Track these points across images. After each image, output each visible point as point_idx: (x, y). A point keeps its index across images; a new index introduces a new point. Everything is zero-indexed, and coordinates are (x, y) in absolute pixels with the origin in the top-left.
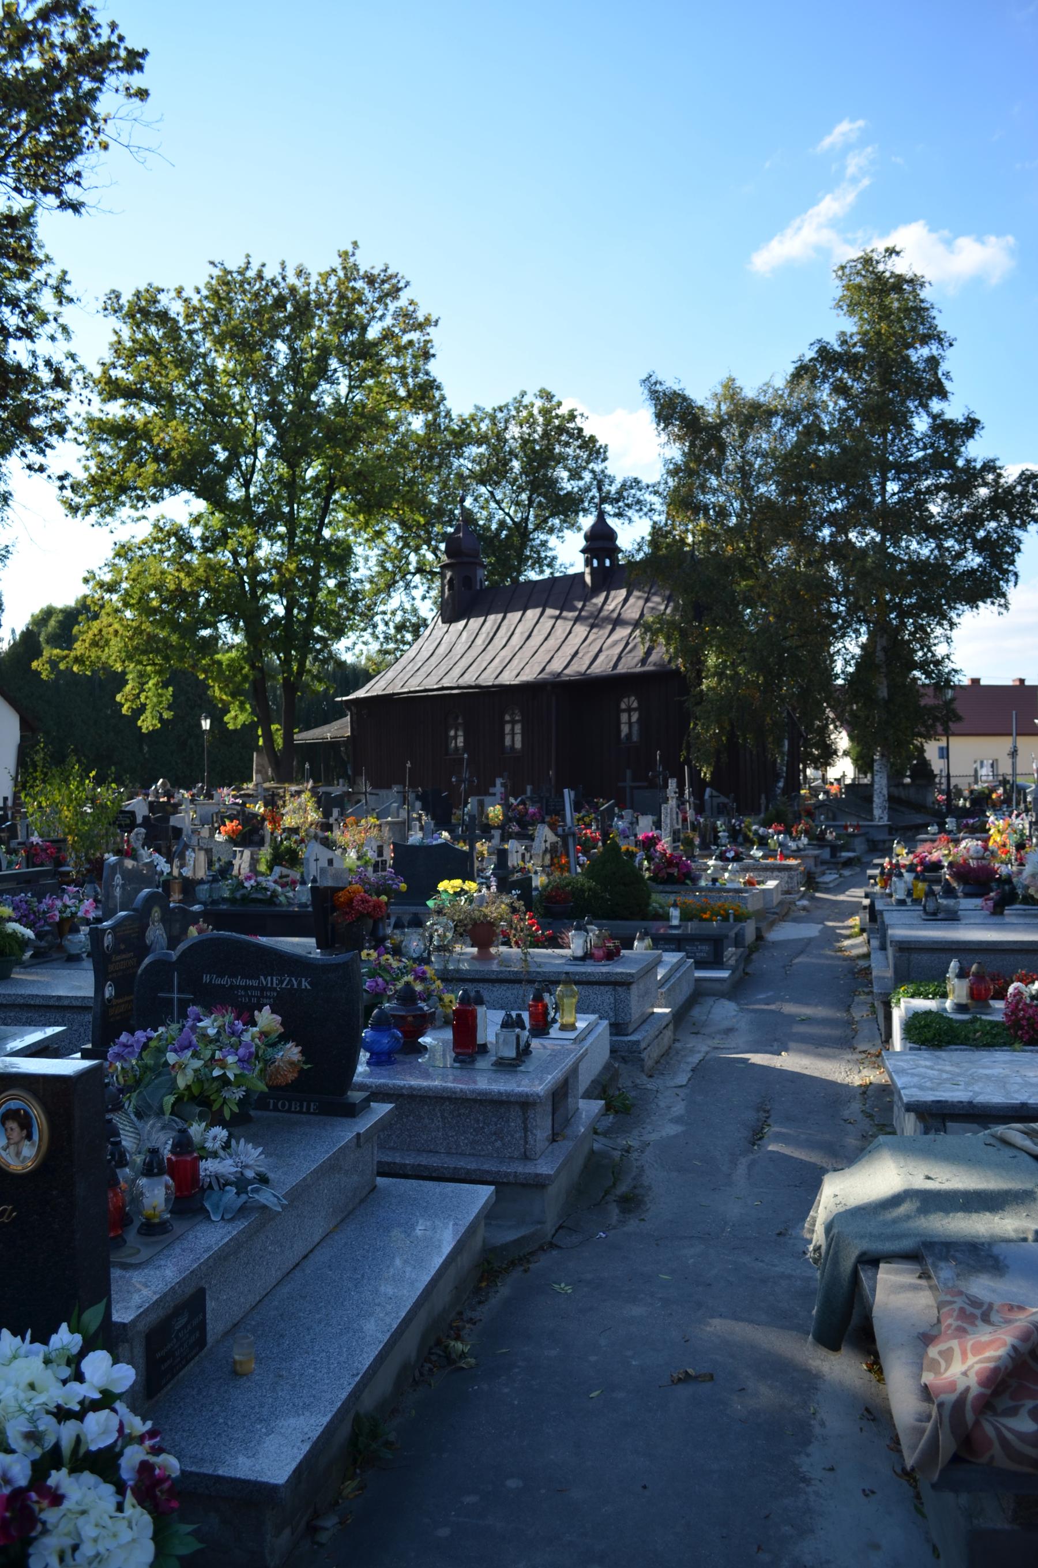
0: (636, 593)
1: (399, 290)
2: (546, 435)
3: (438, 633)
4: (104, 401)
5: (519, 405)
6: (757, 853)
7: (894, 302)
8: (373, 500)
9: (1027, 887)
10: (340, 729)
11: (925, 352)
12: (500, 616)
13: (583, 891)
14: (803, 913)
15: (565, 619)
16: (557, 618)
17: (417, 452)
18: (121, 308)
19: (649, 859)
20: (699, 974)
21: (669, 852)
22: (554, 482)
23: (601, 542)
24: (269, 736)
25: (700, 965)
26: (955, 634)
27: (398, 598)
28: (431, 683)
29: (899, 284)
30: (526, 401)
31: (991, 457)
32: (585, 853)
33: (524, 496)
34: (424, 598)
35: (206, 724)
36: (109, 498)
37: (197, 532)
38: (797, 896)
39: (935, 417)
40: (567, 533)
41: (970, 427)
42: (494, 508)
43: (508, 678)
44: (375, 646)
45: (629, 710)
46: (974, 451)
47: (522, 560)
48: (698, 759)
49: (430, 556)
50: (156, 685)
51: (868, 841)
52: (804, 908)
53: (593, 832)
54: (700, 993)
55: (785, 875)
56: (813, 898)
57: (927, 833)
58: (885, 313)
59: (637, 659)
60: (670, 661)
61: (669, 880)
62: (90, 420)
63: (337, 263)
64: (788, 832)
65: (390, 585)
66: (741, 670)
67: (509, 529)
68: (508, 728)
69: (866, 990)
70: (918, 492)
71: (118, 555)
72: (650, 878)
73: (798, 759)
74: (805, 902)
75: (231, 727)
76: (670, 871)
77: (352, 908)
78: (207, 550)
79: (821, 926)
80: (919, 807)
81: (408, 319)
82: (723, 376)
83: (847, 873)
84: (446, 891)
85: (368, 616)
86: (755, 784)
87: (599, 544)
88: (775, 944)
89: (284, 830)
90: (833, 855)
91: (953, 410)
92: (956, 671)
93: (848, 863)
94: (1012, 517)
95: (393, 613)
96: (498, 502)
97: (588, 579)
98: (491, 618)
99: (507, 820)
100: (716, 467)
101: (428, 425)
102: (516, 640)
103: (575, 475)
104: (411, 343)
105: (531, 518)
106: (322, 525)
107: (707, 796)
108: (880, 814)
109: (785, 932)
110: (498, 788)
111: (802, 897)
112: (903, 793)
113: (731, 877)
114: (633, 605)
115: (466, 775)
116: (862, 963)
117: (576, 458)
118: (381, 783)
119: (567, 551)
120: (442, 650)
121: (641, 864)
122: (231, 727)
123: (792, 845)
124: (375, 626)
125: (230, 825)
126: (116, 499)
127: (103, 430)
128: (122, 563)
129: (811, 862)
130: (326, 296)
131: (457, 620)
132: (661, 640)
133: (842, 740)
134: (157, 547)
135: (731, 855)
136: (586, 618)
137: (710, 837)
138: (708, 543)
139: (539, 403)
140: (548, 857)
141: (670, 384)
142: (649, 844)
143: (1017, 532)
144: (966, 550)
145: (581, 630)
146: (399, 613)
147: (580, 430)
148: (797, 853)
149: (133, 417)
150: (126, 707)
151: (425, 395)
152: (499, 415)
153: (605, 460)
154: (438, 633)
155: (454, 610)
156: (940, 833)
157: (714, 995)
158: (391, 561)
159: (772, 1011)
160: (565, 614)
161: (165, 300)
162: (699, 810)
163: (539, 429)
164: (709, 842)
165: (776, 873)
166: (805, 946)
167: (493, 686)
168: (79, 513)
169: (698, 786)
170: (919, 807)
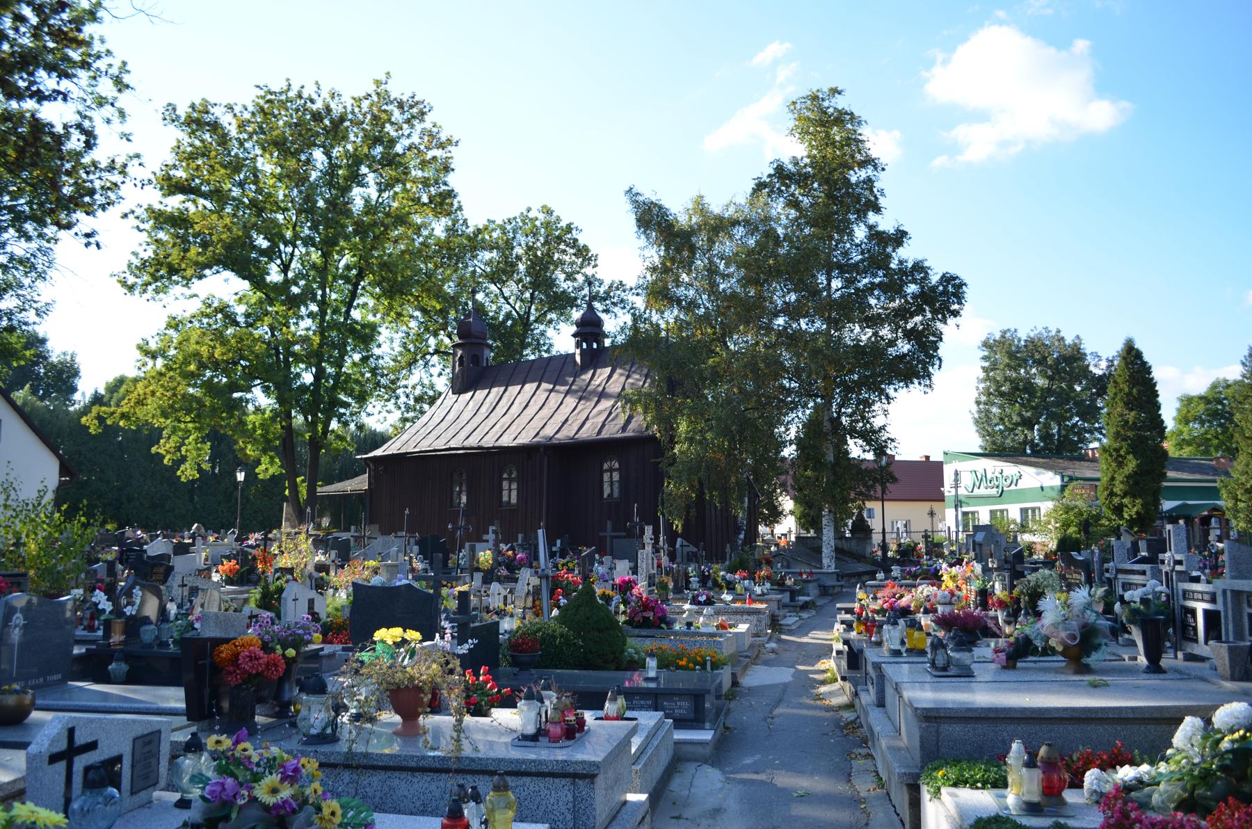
0: (619, 371)
1: (423, 114)
2: (546, 243)
3: (448, 403)
4: (164, 195)
5: (525, 219)
6: (727, 597)
7: (837, 134)
8: (395, 288)
9: (1047, 639)
10: (360, 483)
11: (863, 174)
12: (503, 389)
13: (554, 637)
14: (773, 656)
15: (558, 392)
16: (551, 391)
17: (439, 251)
18: (178, 117)
19: (625, 602)
20: (680, 735)
21: (644, 595)
22: (551, 283)
23: (589, 329)
24: (294, 488)
25: (680, 723)
26: (890, 408)
27: (418, 374)
28: (440, 444)
29: (841, 118)
30: (531, 215)
31: (920, 258)
32: (566, 596)
33: (527, 295)
34: (440, 374)
35: (241, 477)
36: (162, 277)
37: (240, 309)
38: (765, 639)
39: (871, 227)
40: (562, 325)
41: (899, 237)
42: (502, 301)
43: (506, 441)
44: (397, 415)
45: (611, 470)
46: (906, 254)
47: (524, 346)
48: (670, 513)
49: (447, 341)
50: (196, 440)
51: (820, 586)
52: (773, 651)
53: (575, 577)
54: (680, 758)
55: (754, 618)
56: (779, 641)
57: (875, 579)
58: (829, 142)
59: (618, 427)
60: (647, 428)
61: (646, 624)
62: (150, 209)
63: (371, 89)
64: (751, 577)
65: (411, 363)
66: (709, 436)
67: (514, 320)
68: (505, 484)
69: (863, 751)
70: (857, 289)
71: (169, 326)
72: (625, 622)
73: (754, 518)
74: (773, 645)
75: (261, 477)
76: (645, 614)
77: (238, 666)
78: (249, 325)
79: (792, 670)
80: (860, 558)
81: (431, 136)
82: (694, 194)
83: (805, 615)
84: (383, 641)
85: (392, 389)
86: (717, 537)
87: (588, 329)
88: (752, 690)
89: (277, 571)
90: (792, 599)
91: (885, 223)
92: (893, 440)
93: (805, 606)
94: (934, 312)
95: (414, 387)
96: (506, 299)
97: (578, 359)
98: (495, 390)
99: (497, 563)
100: (688, 265)
101: (448, 230)
102: (515, 409)
103: (570, 277)
104: (434, 158)
105: (533, 311)
106: (350, 306)
107: (678, 546)
108: (828, 562)
109: (757, 677)
110: (491, 537)
111: (770, 639)
112: (846, 546)
113: (705, 622)
114: (616, 381)
115: (462, 522)
116: (848, 716)
117: (572, 263)
118: (389, 529)
119: (561, 339)
120: (451, 417)
121: (617, 607)
122: (261, 477)
123: (758, 590)
124: (397, 398)
125: (228, 565)
126: (169, 279)
127: (161, 219)
128: (171, 332)
129: (775, 605)
130: (361, 117)
131: (465, 391)
132: (640, 409)
133: (787, 503)
134: (205, 321)
135: (702, 599)
136: (576, 391)
137: (682, 583)
138: (680, 329)
139: (541, 216)
140: (530, 599)
141: (648, 195)
142: (625, 587)
143: (939, 325)
144: (897, 339)
145: (571, 401)
146: (419, 387)
147: (576, 240)
148: (761, 598)
149: (186, 209)
150: (167, 458)
151: (444, 202)
152: (508, 227)
153: (595, 266)
154: (448, 403)
155: (465, 382)
156: (886, 579)
157: (696, 760)
158: (412, 342)
159: (762, 782)
160: (557, 388)
161: (219, 113)
162: (672, 557)
163: (542, 239)
164: (682, 585)
165: (745, 617)
166: (781, 694)
167: (494, 448)
168: (137, 292)
169: (672, 536)
170: (860, 558)
